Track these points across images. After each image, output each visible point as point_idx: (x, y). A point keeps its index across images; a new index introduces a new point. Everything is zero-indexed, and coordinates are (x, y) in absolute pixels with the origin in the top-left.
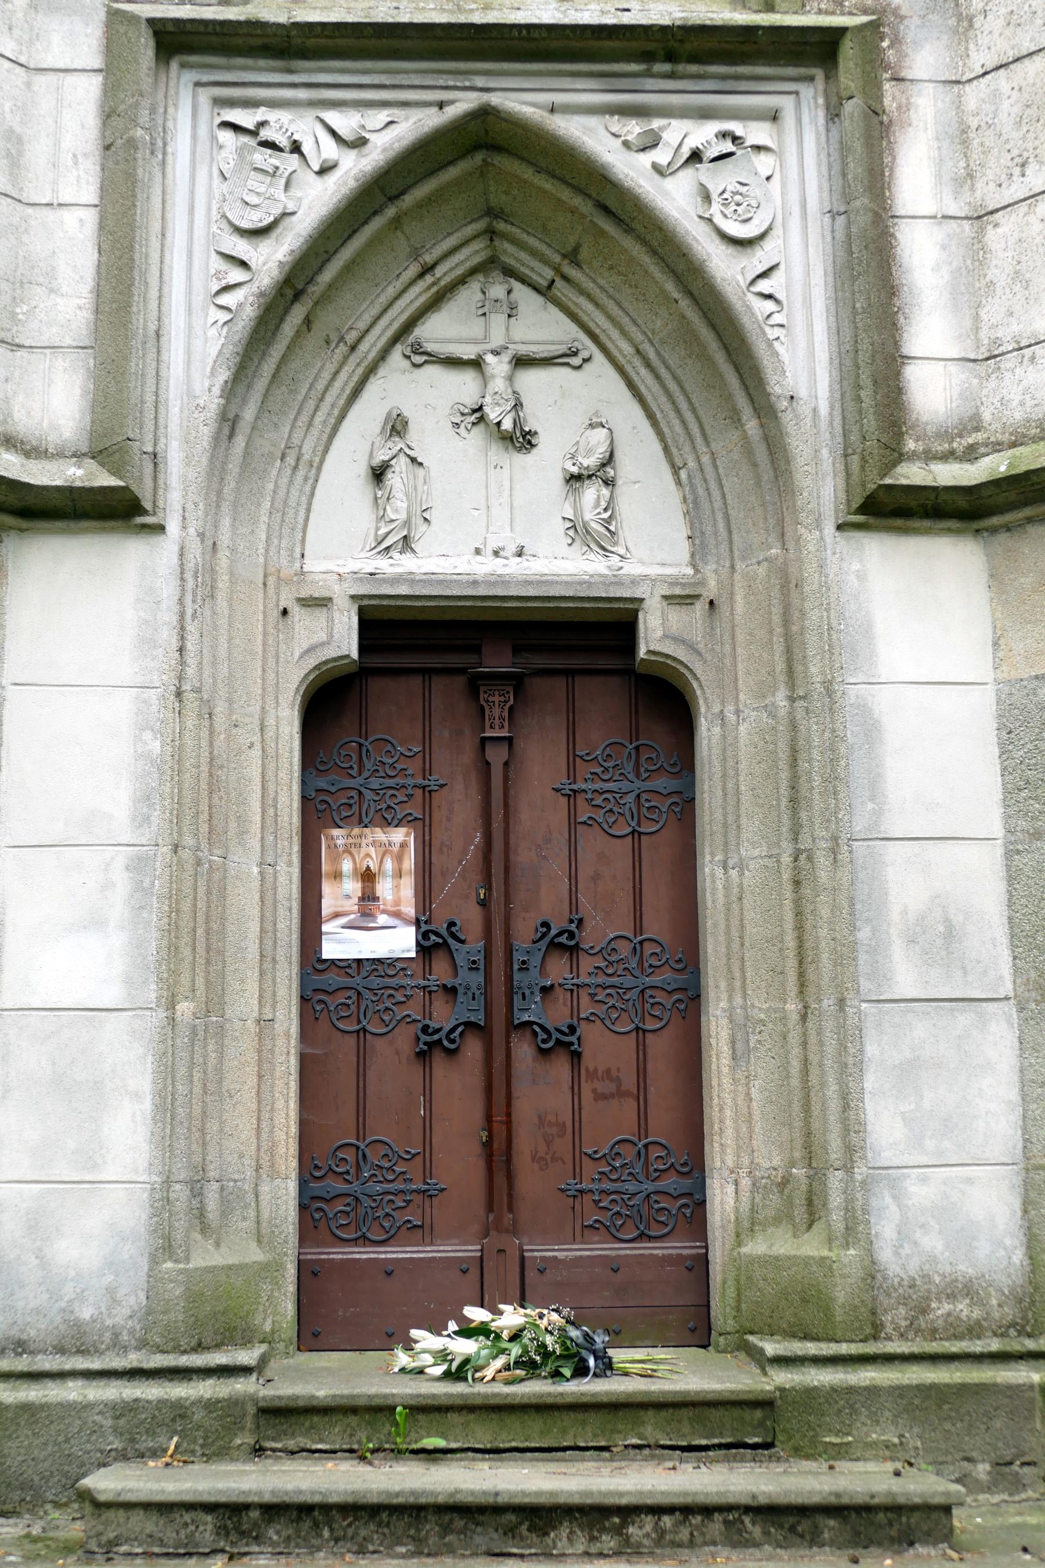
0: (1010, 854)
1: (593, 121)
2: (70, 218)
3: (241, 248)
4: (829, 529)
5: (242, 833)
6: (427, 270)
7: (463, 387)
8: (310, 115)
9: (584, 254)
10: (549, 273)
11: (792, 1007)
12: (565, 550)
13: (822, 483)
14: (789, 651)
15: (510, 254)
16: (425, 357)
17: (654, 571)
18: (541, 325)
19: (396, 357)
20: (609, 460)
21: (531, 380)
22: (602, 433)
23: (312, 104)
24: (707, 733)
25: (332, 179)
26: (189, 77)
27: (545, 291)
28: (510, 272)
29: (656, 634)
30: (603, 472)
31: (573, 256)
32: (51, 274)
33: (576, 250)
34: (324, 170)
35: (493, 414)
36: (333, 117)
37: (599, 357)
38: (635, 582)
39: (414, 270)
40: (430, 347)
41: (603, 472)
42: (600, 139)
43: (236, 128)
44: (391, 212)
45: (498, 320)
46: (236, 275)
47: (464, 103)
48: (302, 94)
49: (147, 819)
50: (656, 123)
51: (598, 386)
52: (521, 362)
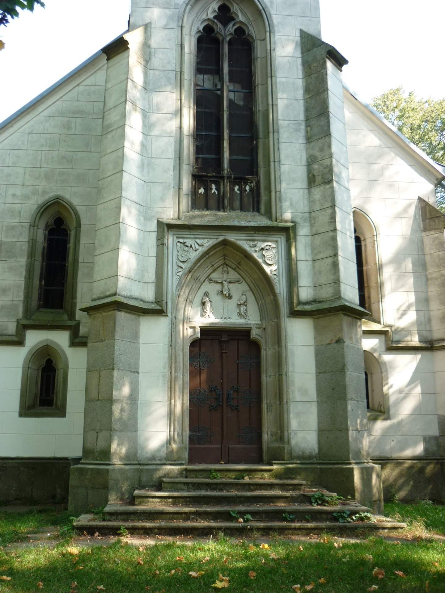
0: (317, 376)
1: (244, 242)
2: (151, 258)
3: (181, 265)
4: (286, 317)
5: (180, 370)
6: (213, 265)
7: (219, 287)
8: (194, 240)
9: (241, 263)
10: (235, 266)
11: (278, 402)
12: (237, 318)
13: (284, 309)
14: (278, 338)
15: (228, 262)
16: (211, 281)
17: (254, 322)
18: (233, 275)
19: (206, 281)
20: (246, 301)
21: (231, 286)
22: (244, 296)
23: (194, 238)
24: (263, 353)
25: (197, 252)
26: (172, 233)
27: (234, 269)
28: (227, 265)
29: (255, 334)
30: (245, 304)
31: (239, 264)
32: (364, 539)
33: (240, 263)
34: (196, 250)
35: (224, 293)
36: (198, 241)
37: (244, 281)
38: (250, 324)
39: (210, 266)
40: (213, 279)
41: (245, 304)
42: (246, 246)
43: (180, 242)
44: (207, 256)
45: (225, 274)
46: (180, 270)
47: (221, 238)
48: (192, 236)
49: (165, 368)
50: (256, 242)
51: (243, 286)
52: (230, 282)
